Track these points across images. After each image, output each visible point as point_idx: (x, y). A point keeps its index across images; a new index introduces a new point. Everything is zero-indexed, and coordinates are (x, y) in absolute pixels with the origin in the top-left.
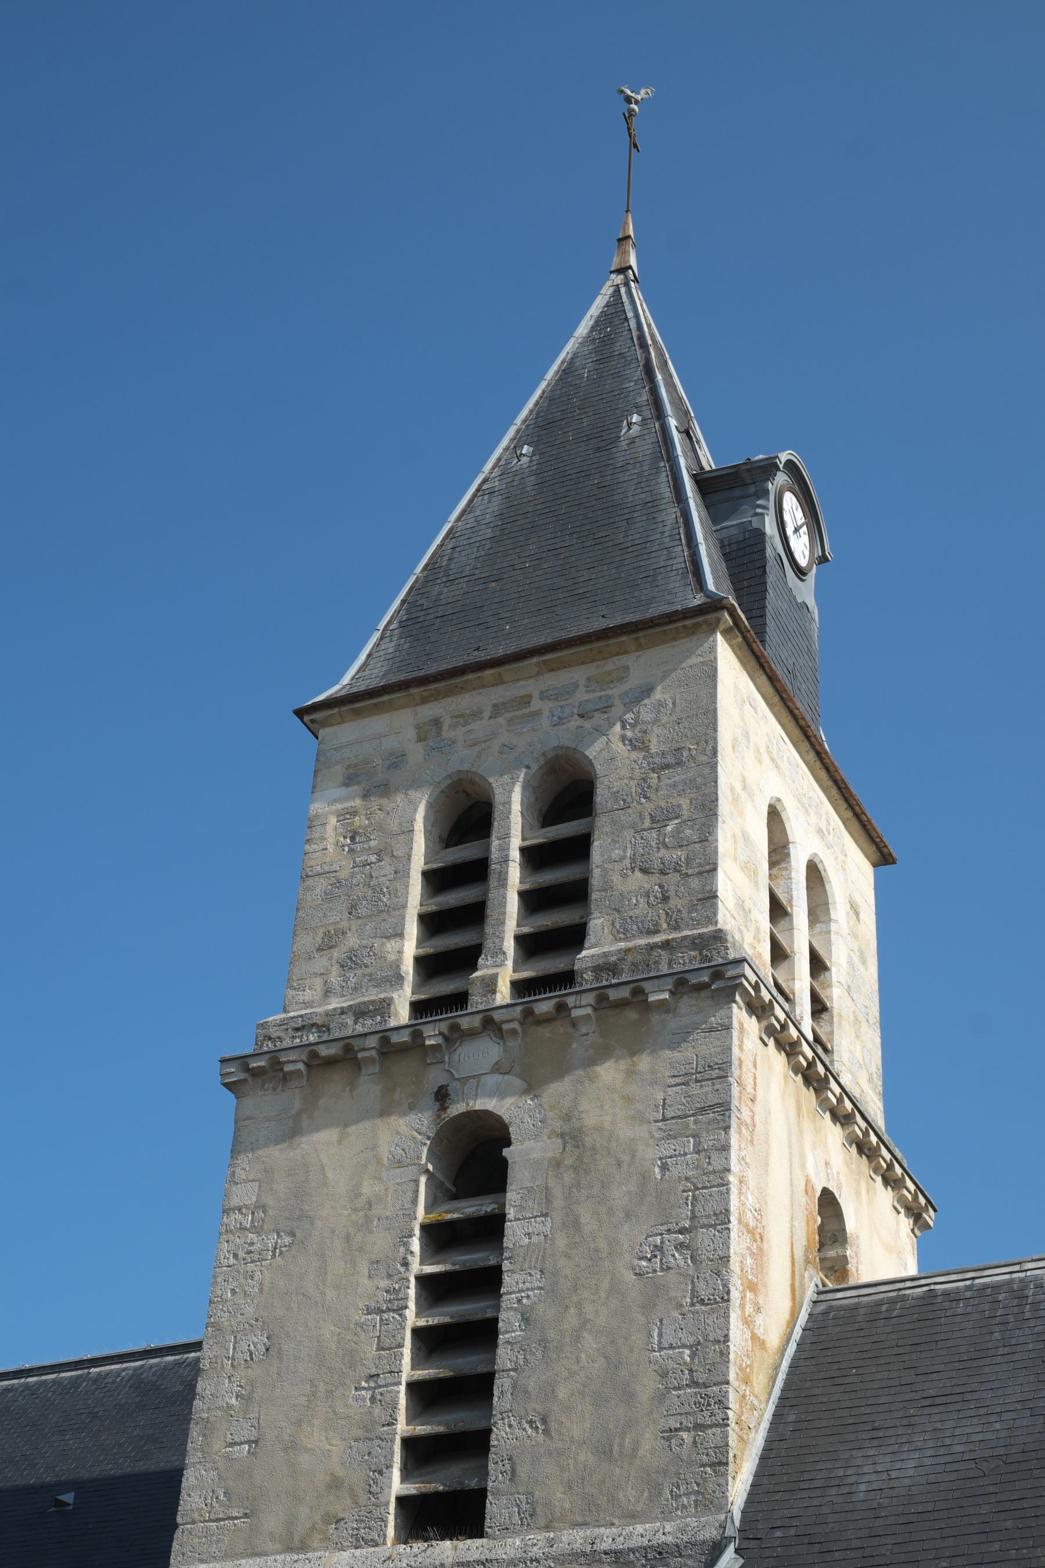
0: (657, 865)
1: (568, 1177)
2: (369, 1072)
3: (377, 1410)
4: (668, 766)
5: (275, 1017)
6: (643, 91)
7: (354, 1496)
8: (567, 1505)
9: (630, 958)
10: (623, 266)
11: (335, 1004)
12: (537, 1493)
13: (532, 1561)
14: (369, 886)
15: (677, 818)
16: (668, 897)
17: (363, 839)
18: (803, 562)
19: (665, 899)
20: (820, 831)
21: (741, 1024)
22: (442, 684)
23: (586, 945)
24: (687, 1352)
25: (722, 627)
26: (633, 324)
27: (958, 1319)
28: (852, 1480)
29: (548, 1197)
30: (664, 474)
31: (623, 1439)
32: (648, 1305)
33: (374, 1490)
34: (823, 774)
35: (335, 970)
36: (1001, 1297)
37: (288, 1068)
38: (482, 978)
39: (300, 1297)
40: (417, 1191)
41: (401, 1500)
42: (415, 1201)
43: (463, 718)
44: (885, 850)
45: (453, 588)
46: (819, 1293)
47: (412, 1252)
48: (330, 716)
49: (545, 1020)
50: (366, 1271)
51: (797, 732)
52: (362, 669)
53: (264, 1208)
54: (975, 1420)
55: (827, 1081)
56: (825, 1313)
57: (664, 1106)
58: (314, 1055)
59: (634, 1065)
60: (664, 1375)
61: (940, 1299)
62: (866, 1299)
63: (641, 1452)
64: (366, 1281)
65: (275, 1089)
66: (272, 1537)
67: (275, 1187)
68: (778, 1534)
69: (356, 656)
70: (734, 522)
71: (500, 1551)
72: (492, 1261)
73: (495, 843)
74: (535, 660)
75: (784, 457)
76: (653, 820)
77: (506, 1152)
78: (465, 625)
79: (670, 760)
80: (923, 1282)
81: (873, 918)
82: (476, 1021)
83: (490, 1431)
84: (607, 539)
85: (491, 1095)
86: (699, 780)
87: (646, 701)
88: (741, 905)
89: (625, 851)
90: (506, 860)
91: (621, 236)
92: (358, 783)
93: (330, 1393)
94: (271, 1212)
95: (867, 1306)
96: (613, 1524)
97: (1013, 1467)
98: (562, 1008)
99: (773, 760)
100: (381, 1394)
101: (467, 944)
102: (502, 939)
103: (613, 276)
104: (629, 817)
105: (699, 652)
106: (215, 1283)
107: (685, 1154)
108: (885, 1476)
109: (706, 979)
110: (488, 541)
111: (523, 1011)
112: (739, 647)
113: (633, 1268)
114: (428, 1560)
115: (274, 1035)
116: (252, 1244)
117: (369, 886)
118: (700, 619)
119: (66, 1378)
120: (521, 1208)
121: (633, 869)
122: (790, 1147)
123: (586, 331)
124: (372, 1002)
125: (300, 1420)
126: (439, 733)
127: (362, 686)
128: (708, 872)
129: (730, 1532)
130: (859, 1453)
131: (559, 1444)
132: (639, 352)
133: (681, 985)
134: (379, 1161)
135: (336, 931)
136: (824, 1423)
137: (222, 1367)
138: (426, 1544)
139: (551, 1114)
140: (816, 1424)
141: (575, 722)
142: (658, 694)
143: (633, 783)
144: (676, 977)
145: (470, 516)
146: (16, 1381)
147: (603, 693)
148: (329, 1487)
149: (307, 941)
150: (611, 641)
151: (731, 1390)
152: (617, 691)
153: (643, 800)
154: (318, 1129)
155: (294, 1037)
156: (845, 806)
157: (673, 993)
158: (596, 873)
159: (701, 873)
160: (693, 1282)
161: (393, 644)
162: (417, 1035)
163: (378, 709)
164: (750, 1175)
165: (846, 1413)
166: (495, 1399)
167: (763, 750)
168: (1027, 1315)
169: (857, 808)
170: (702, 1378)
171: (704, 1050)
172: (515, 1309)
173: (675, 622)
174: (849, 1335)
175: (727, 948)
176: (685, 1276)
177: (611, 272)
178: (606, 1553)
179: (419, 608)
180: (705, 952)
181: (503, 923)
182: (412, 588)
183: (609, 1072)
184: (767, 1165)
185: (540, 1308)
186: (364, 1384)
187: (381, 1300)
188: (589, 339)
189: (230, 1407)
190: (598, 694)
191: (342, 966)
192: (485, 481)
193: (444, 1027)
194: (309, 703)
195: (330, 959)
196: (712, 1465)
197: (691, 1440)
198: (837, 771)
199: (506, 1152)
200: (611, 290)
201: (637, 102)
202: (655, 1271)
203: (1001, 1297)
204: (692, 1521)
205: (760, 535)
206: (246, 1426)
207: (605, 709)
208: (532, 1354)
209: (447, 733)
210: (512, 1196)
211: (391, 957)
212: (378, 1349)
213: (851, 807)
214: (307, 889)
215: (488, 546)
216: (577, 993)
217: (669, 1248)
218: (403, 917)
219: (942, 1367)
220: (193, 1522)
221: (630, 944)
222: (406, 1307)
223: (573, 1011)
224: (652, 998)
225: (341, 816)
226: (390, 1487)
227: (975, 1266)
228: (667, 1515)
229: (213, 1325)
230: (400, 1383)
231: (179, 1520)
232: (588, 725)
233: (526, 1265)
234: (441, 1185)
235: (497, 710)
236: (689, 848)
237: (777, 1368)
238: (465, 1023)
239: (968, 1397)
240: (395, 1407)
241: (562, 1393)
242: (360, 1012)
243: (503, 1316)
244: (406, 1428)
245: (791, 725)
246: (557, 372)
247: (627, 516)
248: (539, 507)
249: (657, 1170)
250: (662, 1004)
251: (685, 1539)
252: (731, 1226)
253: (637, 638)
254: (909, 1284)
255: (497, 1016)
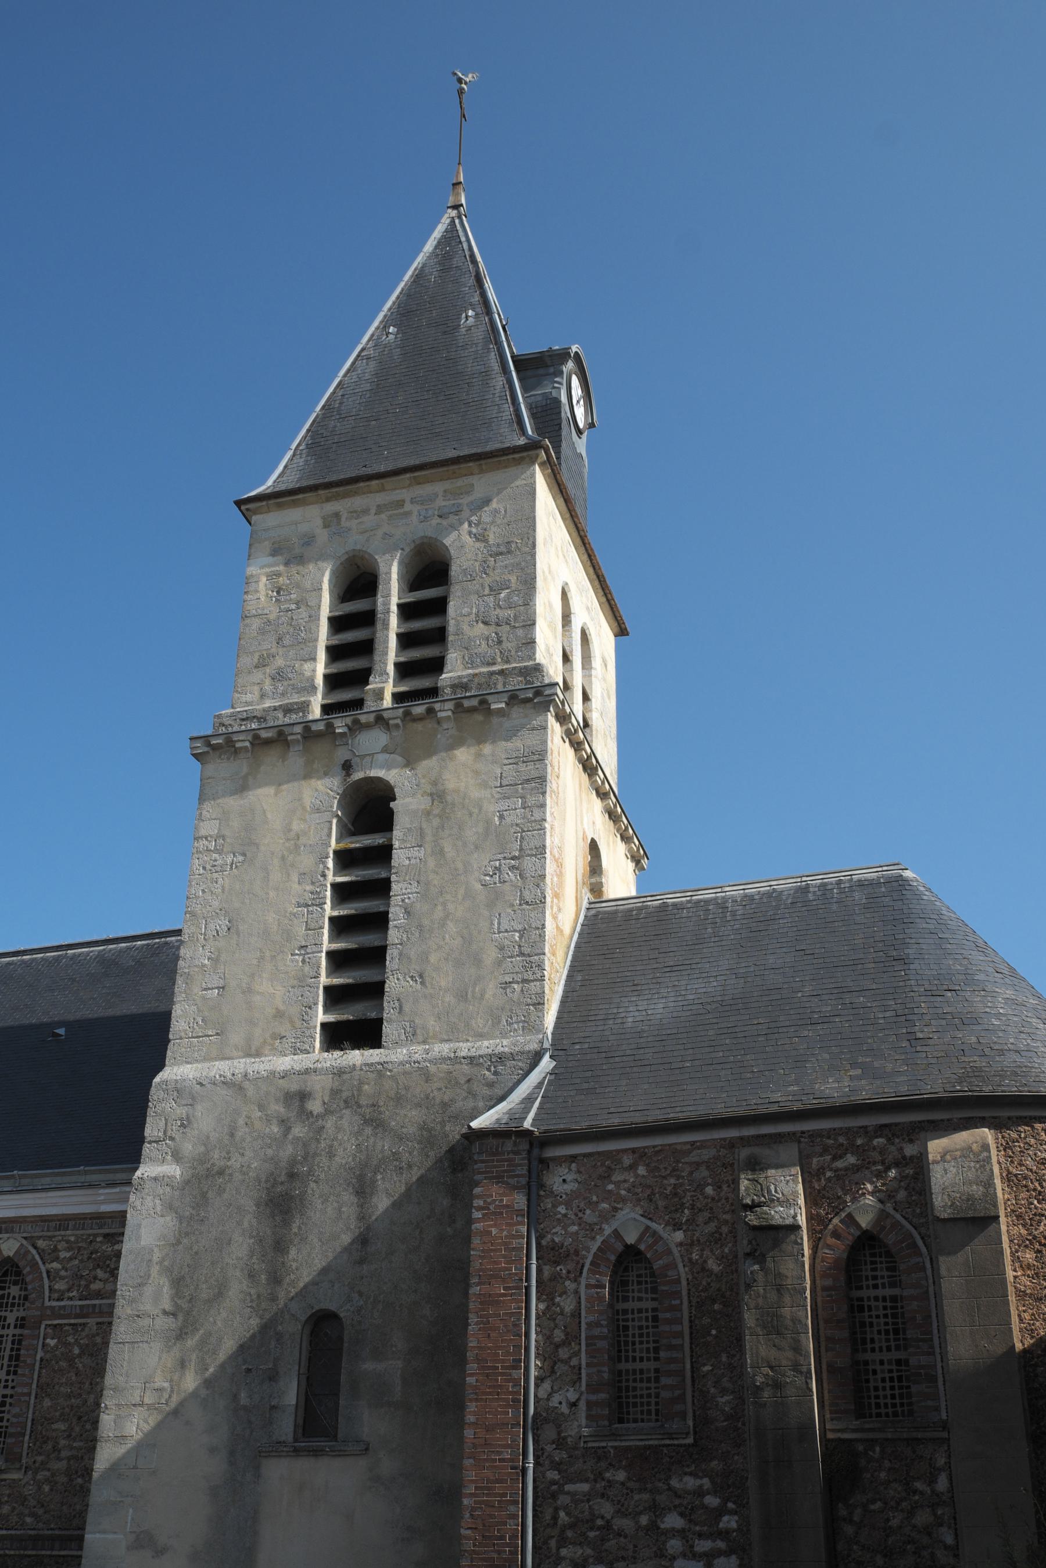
0: (493, 619)
1: (436, 822)
2: (296, 749)
3: (307, 968)
4: (501, 554)
5: (227, 711)
6: (470, 76)
7: (292, 1022)
8: (437, 1029)
9: (476, 680)
10: (457, 203)
11: (268, 704)
12: (417, 1021)
13: (415, 1062)
14: (291, 625)
15: (507, 589)
16: (502, 641)
17: (286, 593)
18: (581, 425)
19: (500, 642)
20: (588, 608)
21: (552, 726)
22: (341, 489)
23: (445, 670)
24: (517, 934)
25: (539, 461)
26: (465, 246)
27: (684, 920)
28: (623, 1015)
29: (422, 834)
30: (493, 353)
31: (474, 988)
32: (491, 905)
33: (306, 1018)
34: (591, 570)
35: (268, 681)
36: (711, 907)
37: (238, 745)
38: (374, 690)
39: (251, 895)
40: (331, 828)
41: (324, 1025)
42: (329, 835)
43: (355, 514)
44: (623, 626)
45: (345, 423)
46: (590, 903)
47: (328, 868)
48: (260, 507)
49: (419, 719)
50: (297, 880)
51: (578, 539)
52: (281, 475)
53: (224, 837)
54: (700, 980)
55: (597, 770)
56: (595, 916)
57: (501, 778)
58: (256, 737)
59: (481, 750)
60: (502, 948)
61: (670, 908)
62: (622, 907)
63: (487, 996)
64: (296, 886)
65: (228, 759)
66: (236, 1048)
67: (231, 823)
68: (577, 1047)
69: (276, 466)
70: (540, 392)
71: (393, 1057)
72: (384, 875)
73: (380, 600)
74: (408, 475)
75: (574, 348)
76: (491, 589)
77: (392, 804)
78: (355, 449)
79: (503, 549)
80: (658, 897)
81: (614, 669)
82: (371, 718)
83: (385, 982)
84: (454, 396)
85: (381, 767)
86: (523, 564)
87: (486, 509)
88: (548, 650)
89: (471, 609)
90: (388, 611)
91: (454, 182)
92: (282, 554)
93: (273, 957)
94: (228, 840)
95: (622, 911)
96: (468, 1041)
97: (727, 1008)
98: (431, 711)
99: (564, 557)
100: (309, 958)
101: (361, 667)
102: (386, 664)
103: (450, 211)
104: (474, 586)
105: (523, 477)
106: (190, 886)
107: (516, 809)
108: (644, 1013)
109: (531, 696)
110: (368, 392)
111: (403, 712)
112: (549, 476)
113: (480, 881)
114: (345, 1062)
115: (226, 723)
116: (216, 860)
117: (291, 625)
118: (525, 454)
119: (51, 957)
120: (403, 841)
121: (477, 622)
122: (576, 810)
123: (431, 249)
124: (296, 703)
125: (253, 974)
126: (339, 522)
127: (282, 487)
128: (529, 625)
129: (546, 1045)
130: (626, 999)
131: (431, 991)
132: (471, 266)
133: (513, 698)
134: (304, 808)
135: (268, 656)
136: (601, 981)
137: (198, 940)
138: (342, 1053)
139: (423, 781)
140: (596, 982)
141: (436, 521)
142: (494, 504)
143: (477, 564)
144: (510, 693)
145: (353, 374)
146: (15, 958)
147: (456, 502)
148: (275, 1017)
149: (246, 661)
150: (462, 466)
151: (546, 958)
152: (465, 500)
153: (484, 576)
154: (260, 787)
155: (241, 725)
156: (602, 593)
157: (507, 704)
158: (452, 623)
159: (524, 626)
160: (521, 891)
161: (303, 460)
162: (330, 726)
163: (295, 504)
164: (556, 823)
165: (615, 975)
166: (388, 963)
167: (559, 549)
168: (729, 918)
169: (609, 596)
170: (527, 950)
171: (529, 742)
172: (400, 906)
173: (507, 455)
174: (612, 929)
175: (543, 676)
176: (516, 887)
177: (448, 207)
178: (464, 1058)
179: (320, 436)
180: (528, 678)
181: (387, 654)
182: (314, 421)
183: (463, 755)
184: (564, 819)
185: (418, 905)
186: (297, 952)
187: (307, 898)
188: (433, 254)
189: (204, 965)
190: (453, 502)
191: (273, 679)
192: (363, 350)
193: (349, 720)
194: (246, 496)
195: (265, 674)
196: (533, 1005)
197: (520, 989)
198: (600, 569)
199: (392, 804)
200: (448, 221)
201: (466, 83)
202: (495, 883)
203: (711, 907)
204: (521, 1039)
205: (557, 402)
206: (216, 977)
207: (457, 513)
208: (412, 934)
209: (344, 523)
210: (397, 833)
211: (308, 674)
212: (306, 930)
213: (605, 595)
214: (246, 625)
215: (368, 396)
216: (441, 701)
217: (505, 869)
218: (316, 647)
219: (675, 949)
220: (181, 1038)
221: (477, 671)
222: (325, 903)
223: (439, 713)
224: (493, 706)
225: (270, 576)
226: (317, 1017)
227: (692, 888)
228: (504, 1035)
229: (190, 913)
230: (322, 952)
231: (171, 1036)
232: (445, 522)
233: (407, 878)
234: (346, 825)
235: (380, 509)
236: (517, 609)
237: (569, 948)
238: (363, 719)
239: (694, 966)
240: (319, 967)
241: (433, 958)
242: (287, 710)
243: (392, 910)
244: (326, 980)
245: (575, 534)
246: (412, 276)
247: (468, 381)
248: (404, 371)
249: (496, 819)
250: (500, 712)
251: (517, 1049)
252: (546, 855)
253: (481, 465)
254: (649, 899)
255: (386, 715)
